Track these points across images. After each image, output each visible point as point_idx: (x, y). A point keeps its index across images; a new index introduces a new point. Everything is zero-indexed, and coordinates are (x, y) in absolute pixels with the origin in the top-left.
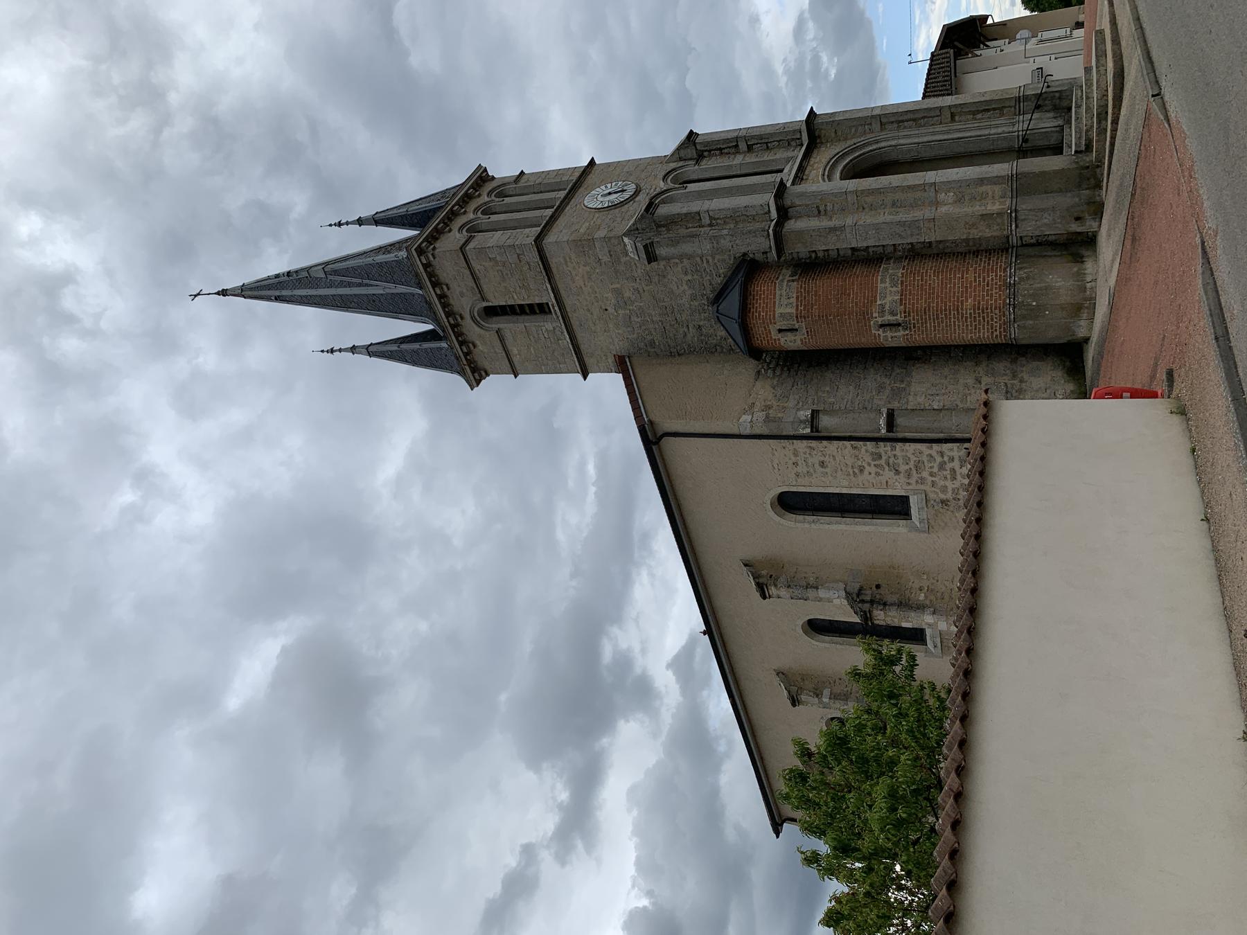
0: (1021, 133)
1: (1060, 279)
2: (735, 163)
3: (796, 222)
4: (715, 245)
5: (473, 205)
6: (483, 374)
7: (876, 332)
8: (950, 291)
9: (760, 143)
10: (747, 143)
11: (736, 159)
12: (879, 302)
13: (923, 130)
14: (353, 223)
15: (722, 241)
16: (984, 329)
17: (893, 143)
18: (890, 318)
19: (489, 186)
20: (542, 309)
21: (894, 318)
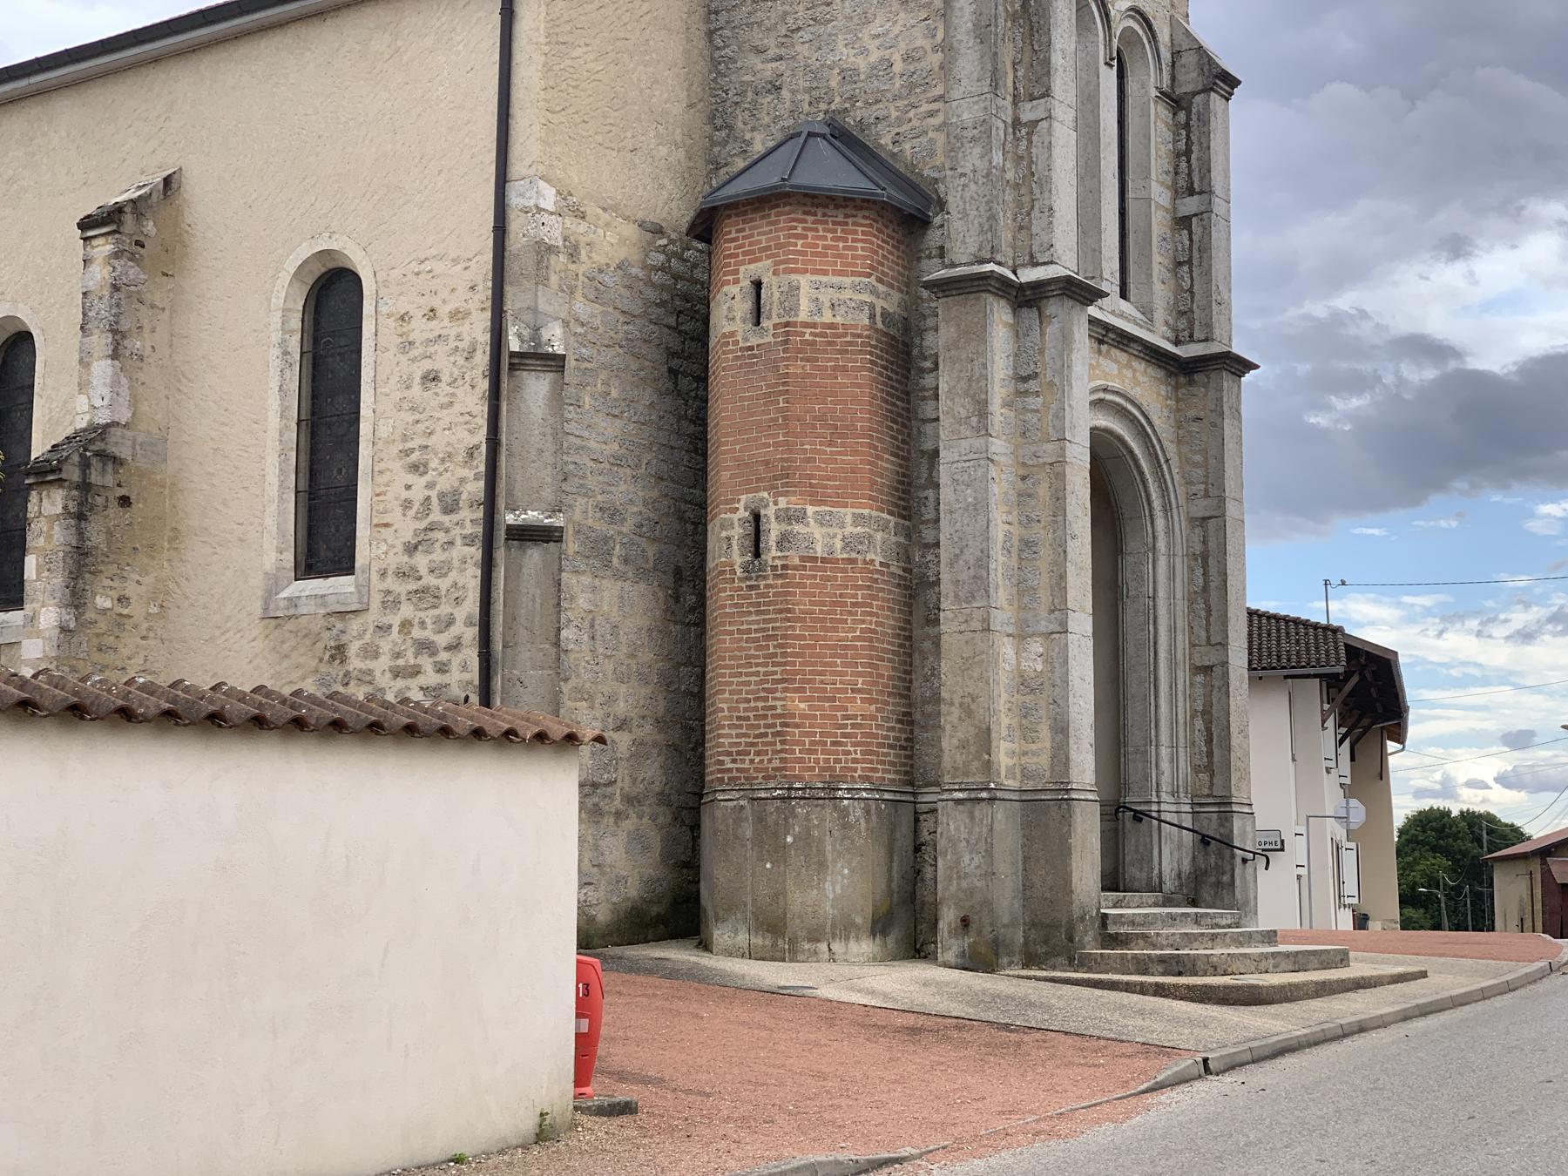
2: (1154, 184)
4: (969, 134)
7: (742, 503)
9: (1191, 249)
10: (1195, 215)
12: (810, 510)
13: (1181, 606)
15: (977, 150)
17: (1161, 544)
21: (773, 544)
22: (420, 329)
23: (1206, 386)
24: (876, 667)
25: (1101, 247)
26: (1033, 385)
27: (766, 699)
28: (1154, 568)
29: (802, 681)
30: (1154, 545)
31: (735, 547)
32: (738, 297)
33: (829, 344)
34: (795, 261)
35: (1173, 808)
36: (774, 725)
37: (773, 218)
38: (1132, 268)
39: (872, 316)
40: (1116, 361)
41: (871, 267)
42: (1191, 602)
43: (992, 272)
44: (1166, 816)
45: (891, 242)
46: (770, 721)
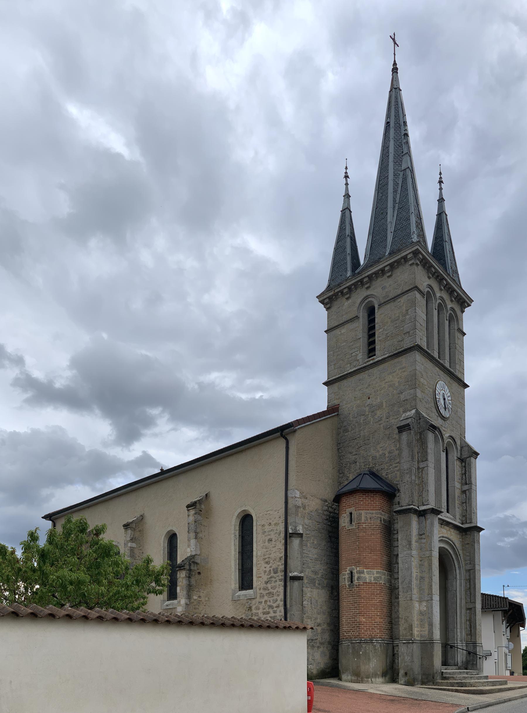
1: (373, 666)
2: (456, 483)
3: (416, 521)
4: (406, 472)
6: (328, 306)
8: (370, 609)
12: (365, 570)
13: (463, 593)
16: (348, 627)
17: (458, 577)
19: (457, 309)
20: (371, 351)
22: (267, 528)
26: (423, 536)
29: (364, 613)
30: (456, 578)
32: (346, 517)
33: (370, 528)
35: (461, 645)
40: (446, 529)
42: (466, 592)
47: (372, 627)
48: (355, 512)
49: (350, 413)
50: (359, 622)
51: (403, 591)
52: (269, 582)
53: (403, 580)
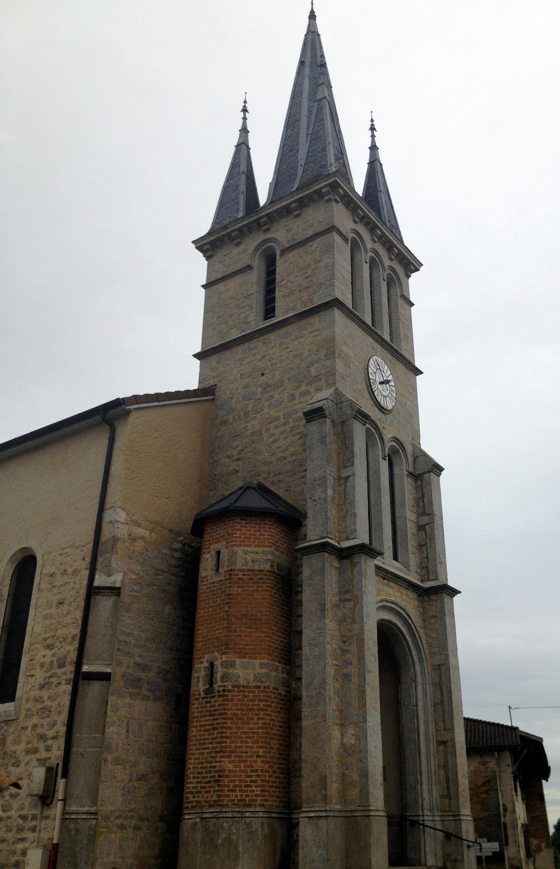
0: (421, 818)
2: (407, 511)
3: (335, 568)
4: (317, 482)
5: (382, 252)
6: (208, 254)
7: (206, 659)
10: (427, 524)
11: (339, 370)
12: (238, 661)
13: (430, 710)
14: (373, 142)
15: (321, 489)
16: (197, 783)
17: (419, 679)
18: (219, 675)
19: (401, 271)
20: (269, 311)
21: (219, 679)
22: (59, 580)
23: (436, 601)
24: (269, 743)
25: (383, 536)
27: (211, 762)
28: (416, 690)
29: (230, 752)
30: (415, 680)
31: (201, 682)
32: (210, 559)
34: (235, 541)
35: (431, 818)
36: (214, 777)
37: (227, 522)
38: (399, 548)
39: (272, 566)
41: (272, 543)
43: (326, 542)
44: (428, 823)
45: (283, 533)
46: (213, 774)
47: (247, 781)
48: (226, 551)
49: (232, 397)
50: (220, 771)
51: (310, 704)
52: (46, 686)
53: (310, 680)
